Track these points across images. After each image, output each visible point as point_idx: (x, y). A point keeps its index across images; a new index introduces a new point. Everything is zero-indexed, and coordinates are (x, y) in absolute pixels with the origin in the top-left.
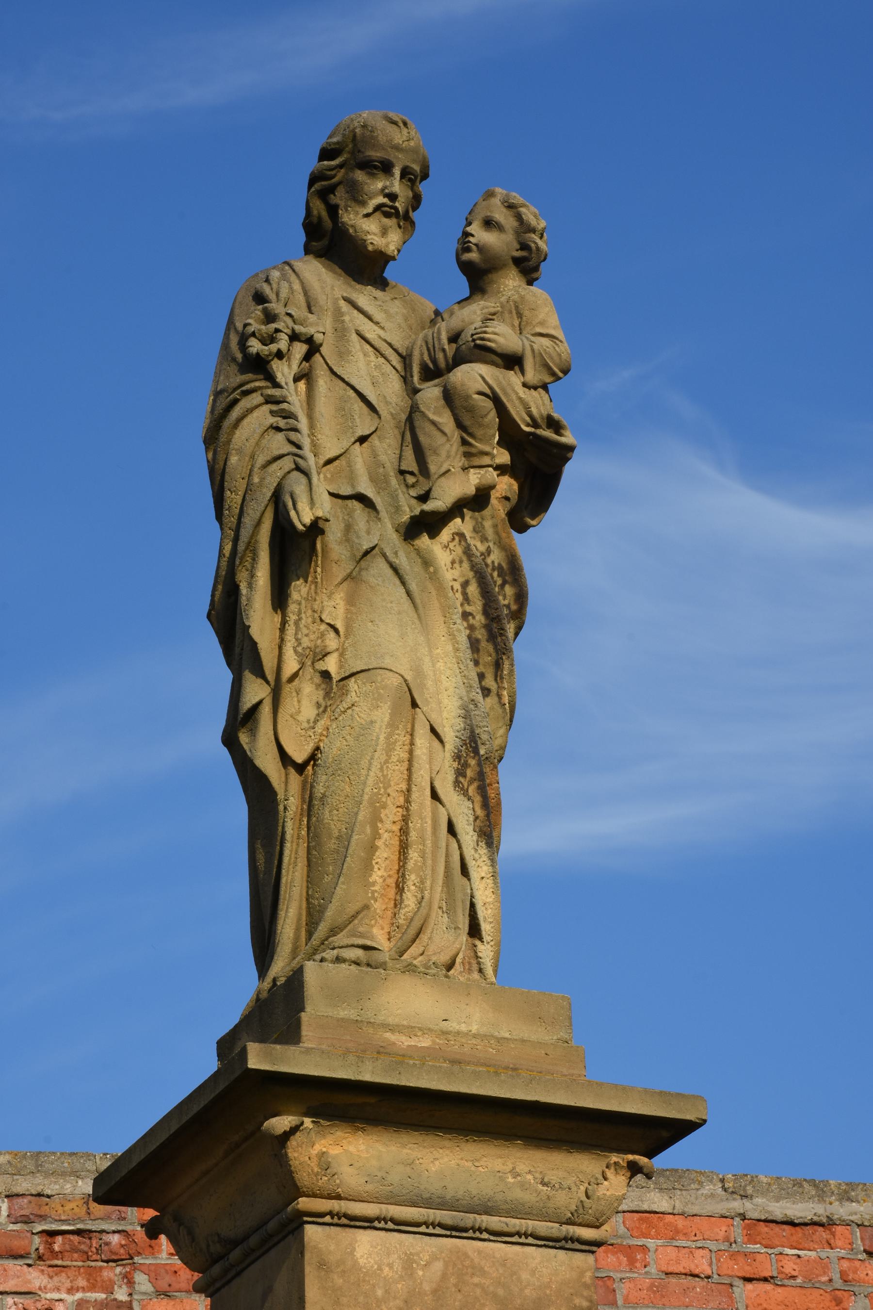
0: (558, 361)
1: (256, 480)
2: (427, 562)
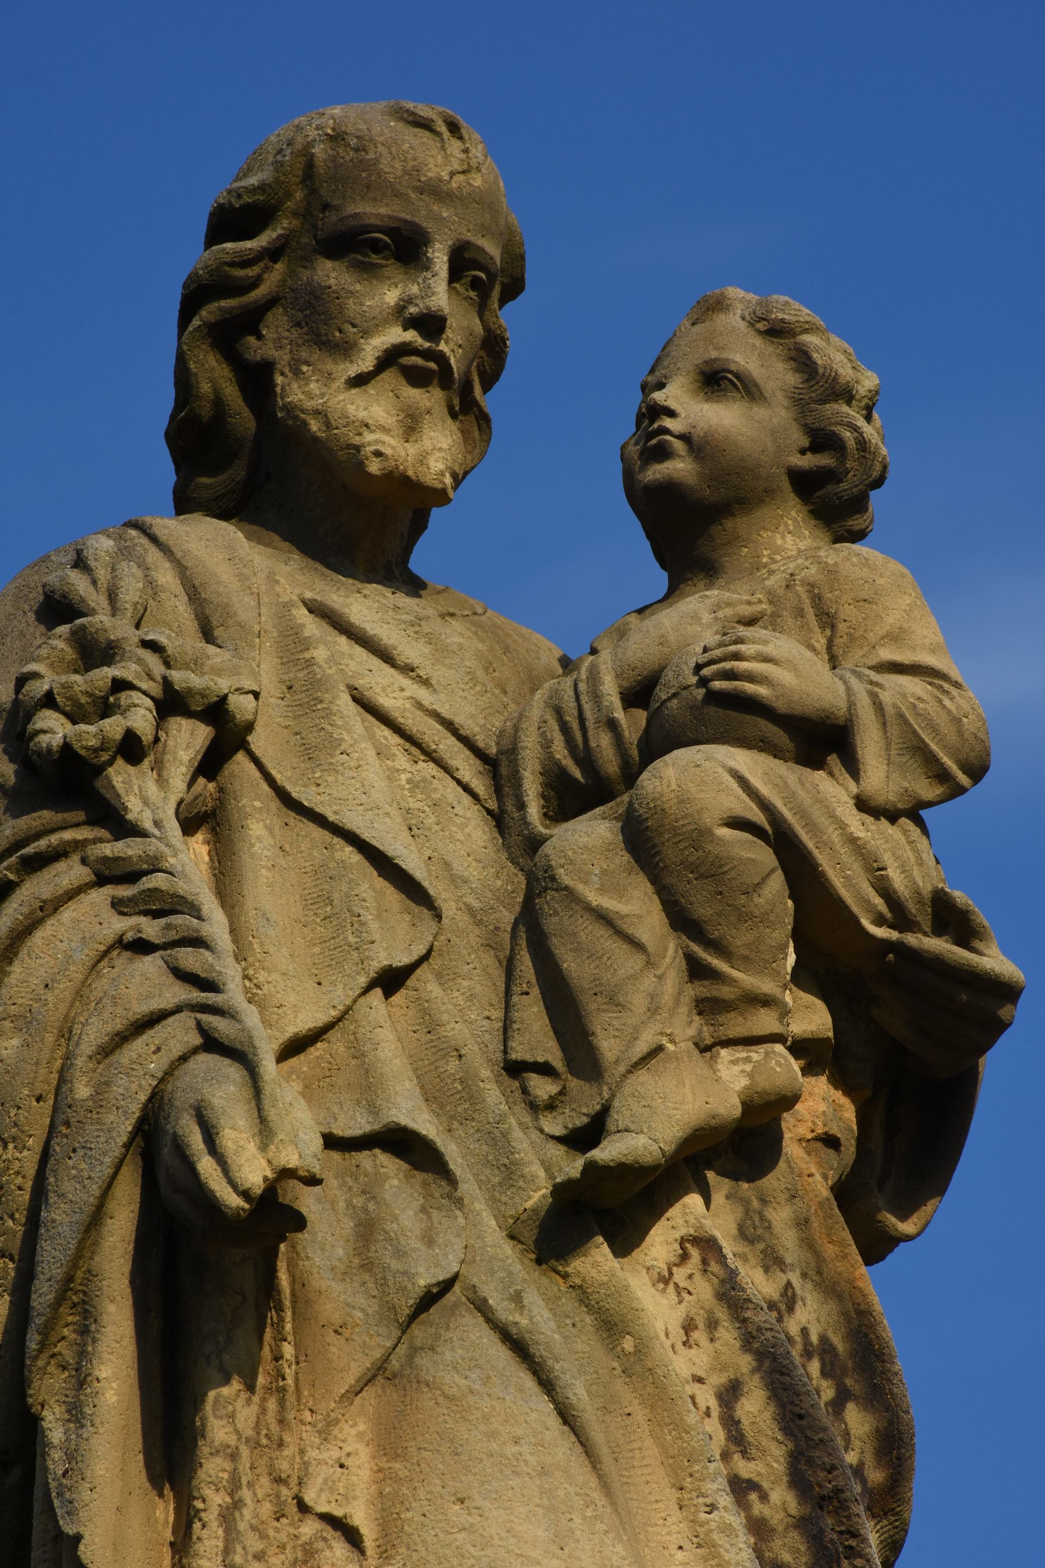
0: (952, 738)
1: (82, 1091)
2: (612, 1324)
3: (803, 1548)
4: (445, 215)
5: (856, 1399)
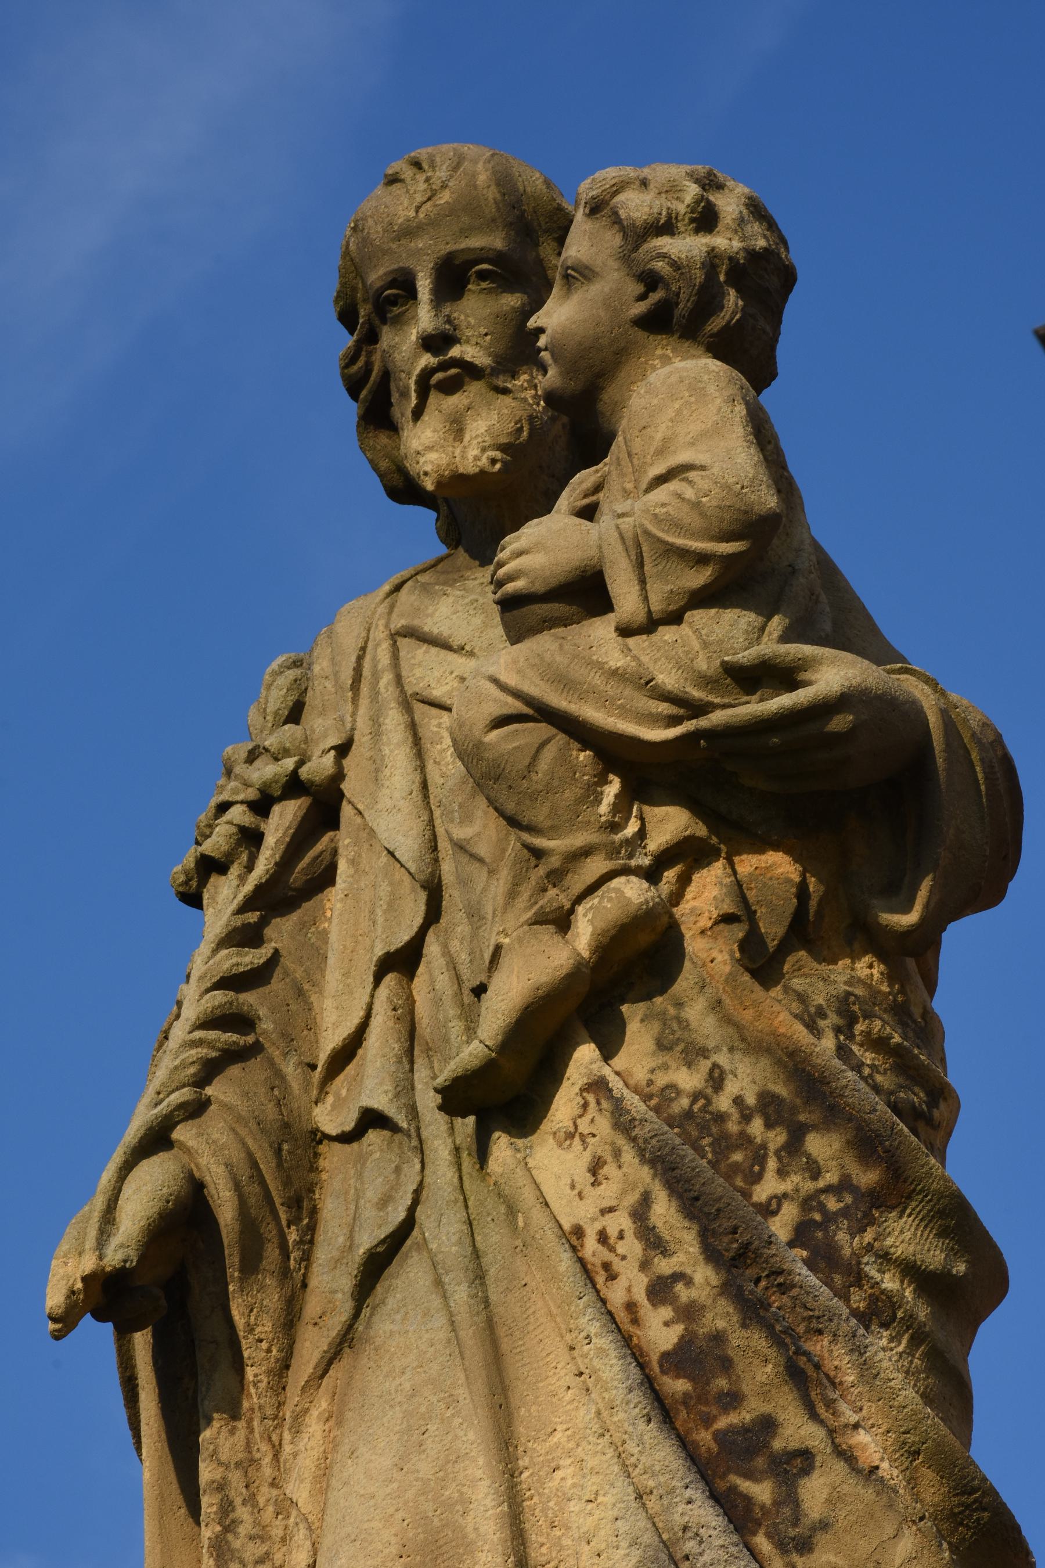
3: (731, 1310)
4: (420, 246)
5: (814, 1127)
